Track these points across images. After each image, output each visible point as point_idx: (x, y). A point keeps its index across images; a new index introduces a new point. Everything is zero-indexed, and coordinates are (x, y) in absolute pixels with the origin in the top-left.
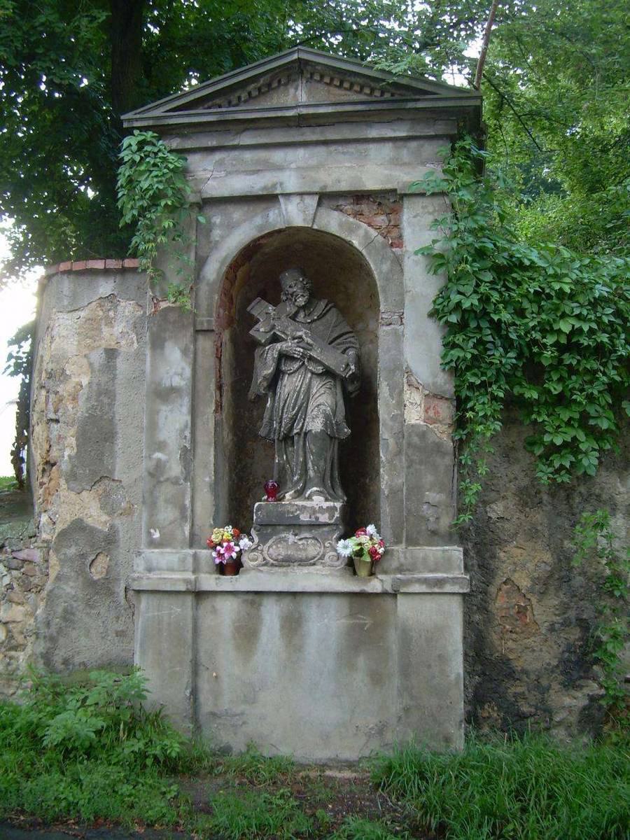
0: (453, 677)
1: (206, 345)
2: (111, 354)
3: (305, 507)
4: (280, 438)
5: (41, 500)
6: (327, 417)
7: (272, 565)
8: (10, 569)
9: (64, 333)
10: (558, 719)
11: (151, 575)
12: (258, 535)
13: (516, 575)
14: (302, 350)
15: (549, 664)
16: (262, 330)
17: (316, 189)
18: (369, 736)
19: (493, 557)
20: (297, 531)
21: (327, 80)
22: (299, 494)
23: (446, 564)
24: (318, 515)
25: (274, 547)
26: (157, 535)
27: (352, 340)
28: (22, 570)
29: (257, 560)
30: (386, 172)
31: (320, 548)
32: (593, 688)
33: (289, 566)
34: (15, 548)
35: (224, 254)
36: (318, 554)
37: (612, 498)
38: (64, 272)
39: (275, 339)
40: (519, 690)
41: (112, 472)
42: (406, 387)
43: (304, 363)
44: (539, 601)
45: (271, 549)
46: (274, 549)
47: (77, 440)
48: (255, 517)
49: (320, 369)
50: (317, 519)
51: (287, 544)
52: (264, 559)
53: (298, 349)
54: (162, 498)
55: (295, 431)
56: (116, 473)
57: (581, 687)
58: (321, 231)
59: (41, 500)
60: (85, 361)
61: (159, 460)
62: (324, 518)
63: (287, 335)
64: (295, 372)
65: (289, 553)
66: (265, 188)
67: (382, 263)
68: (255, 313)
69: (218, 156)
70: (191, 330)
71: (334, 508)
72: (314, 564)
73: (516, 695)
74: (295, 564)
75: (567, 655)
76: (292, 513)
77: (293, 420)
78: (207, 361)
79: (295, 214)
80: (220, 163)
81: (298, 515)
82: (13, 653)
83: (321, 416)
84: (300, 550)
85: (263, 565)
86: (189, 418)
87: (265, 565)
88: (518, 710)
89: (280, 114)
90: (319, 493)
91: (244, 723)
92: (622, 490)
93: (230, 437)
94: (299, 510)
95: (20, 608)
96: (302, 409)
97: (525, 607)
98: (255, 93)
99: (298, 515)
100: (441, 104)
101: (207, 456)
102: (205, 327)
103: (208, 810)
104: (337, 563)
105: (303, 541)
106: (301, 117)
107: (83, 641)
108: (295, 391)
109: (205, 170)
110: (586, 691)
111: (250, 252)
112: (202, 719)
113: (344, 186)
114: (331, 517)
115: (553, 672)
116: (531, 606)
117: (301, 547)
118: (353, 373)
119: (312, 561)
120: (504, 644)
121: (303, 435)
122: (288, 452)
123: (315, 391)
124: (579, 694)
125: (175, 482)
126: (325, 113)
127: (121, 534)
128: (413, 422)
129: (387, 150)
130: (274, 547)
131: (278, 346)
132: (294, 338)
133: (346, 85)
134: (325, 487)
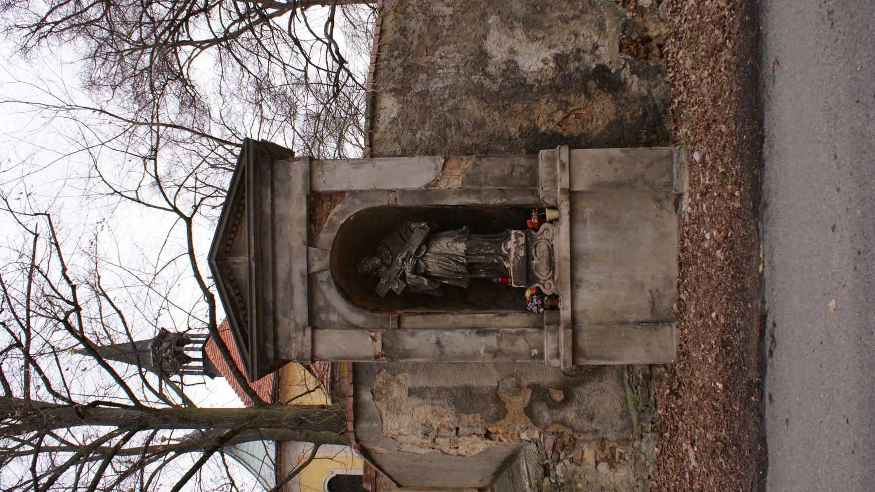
0: (622, 154)
1: (408, 321)
2: (411, 392)
3: (515, 253)
5: (511, 440)
6: (456, 241)
7: (553, 273)
8: (559, 461)
9: (397, 425)
10: (646, 93)
11: (562, 354)
13: (556, 120)
15: (612, 99)
16: (397, 286)
17: (305, 248)
18: (661, 208)
19: (544, 134)
21: (230, 242)
22: (506, 258)
23: (551, 160)
24: (520, 243)
26: (535, 351)
27: (404, 229)
28: (560, 451)
29: (550, 284)
30: (295, 201)
32: (626, 73)
34: (545, 457)
35: (347, 311)
37: (505, 63)
38: (355, 427)
39: (403, 277)
40: (628, 117)
41: (492, 388)
42: (437, 188)
43: (420, 258)
44: (572, 106)
46: (542, 273)
47: (470, 414)
49: (424, 247)
50: (522, 245)
52: (550, 278)
54: (510, 348)
56: (493, 385)
57: (625, 79)
58: (333, 245)
59: (511, 440)
60: (417, 409)
61: (485, 351)
62: (522, 241)
63: (401, 269)
64: (425, 264)
66: (303, 283)
67: (355, 205)
68: (386, 291)
69: (280, 316)
70: (398, 331)
71: (516, 234)
72: (552, 245)
73: (632, 118)
75: (605, 89)
76: (519, 261)
77: (457, 262)
78: (419, 320)
79: (321, 262)
80: (285, 314)
81: (521, 257)
82: (617, 456)
83: (455, 244)
84: (543, 255)
85: (554, 279)
86: (458, 331)
87: (553, 277)
88: (641, 117)
89: (254, 272)
90: (505, 245)
91: (657, 290)
92: (499, 57)
95: (585, 452)
96: (450, 257)
97: (576, 114)
98: (237, 291)
99: (521, 257)
100: (251, 165)
101: (482, 318)
104: (551, 230)
105: (537, 253)
106: (256, 259)
107: (607, 405)
108: (438, 263)
109: (289, 325)
110: (627, 76)
111: (347, 296)
112: (655, 319)
113: (304, 230)
114: (521, 236)
115: (616, 97)
116: (574, 110)
120: (598, 126)
123: (438, 250)
124: (630, 81)
125: (500, 340)
126: (232, 306)
127: (534, 380)
128: (460, 183)
129: (280, 202)
131: (408, 274)
132: (403, 264)
133: (234, 229)
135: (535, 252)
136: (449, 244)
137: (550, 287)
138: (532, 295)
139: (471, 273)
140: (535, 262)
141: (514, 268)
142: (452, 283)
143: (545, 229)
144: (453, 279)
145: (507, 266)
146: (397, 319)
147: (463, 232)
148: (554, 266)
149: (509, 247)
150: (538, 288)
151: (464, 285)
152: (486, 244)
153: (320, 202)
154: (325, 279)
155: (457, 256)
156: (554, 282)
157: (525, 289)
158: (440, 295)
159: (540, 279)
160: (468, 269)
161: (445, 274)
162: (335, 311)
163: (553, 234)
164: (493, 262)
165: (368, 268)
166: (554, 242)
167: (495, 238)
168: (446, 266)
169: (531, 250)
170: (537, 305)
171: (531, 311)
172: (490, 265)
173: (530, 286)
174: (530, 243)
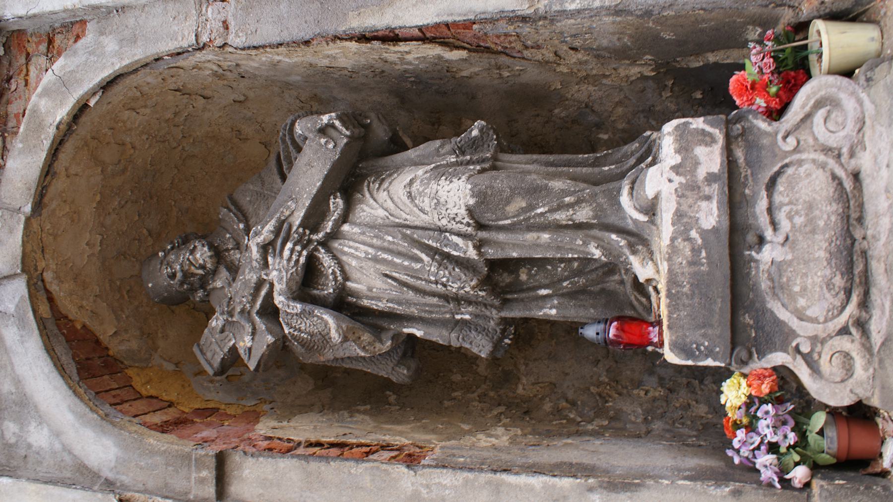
3: (679, 215)
4: (497, 302)
6: (440, 172)
7: (865, 304)
12: (762, 354)
14: (289, 245)
20: (751, 238)
24: (702, 173)
25: (802, 302)
29: (847, 356)
31: (800, 163)
33: (864, 253)
35: (70, 417)
36: (823, 166)
39: (270, 312)
45: (809, 313)
48: (710, 362)
49: (337, 204)
50: (711, 178)
51: (790, 263)
52: (844, 331)
53: (286, 253)
55: (472, 253)
65: (822, 254)
71: (682, 134)
72: (856, 176)
74: (858, 234)
76: (695, 251)
77: (444, 258)
81: (703, 233)
83: (434, 186)
84: (811, 221)
85: (865, 332)
87: (862, 325)
93: (500, 430)
94: (687, 231)
99: (703, 233)
102: (208, 474)
103: (263, 496)
104: (849, 104)
105: (781, 216)
108: (375, 260)
114: (706, 139)
117: (799, 220)
118: (339, 118)
119: (848, 185)
121: (483, 234)
122: (532, 283)
123: (381, 213)
130: (802, 302)
131: (279, 300)
132: (266, 265)
134: (622, 176)
135: (770, 210)
136: (416, 186)
137: (849, 371)
138: (750, 402)
139: (505, 303)
140: (767, 255)
141: (672, 281)
142: (438, 336)
143: (818, 105)
144: (443, 323)
145: (643, 272)
146: (212, 463)
147: (475, 145)
148: (866, 272)
149: (650, 192)
150: (783, 375)
151: (481, 347)
152: (557, 185)
153: (22, 60)
154: (11, 307)
155: (441, 230)
156: (867, 348)
157: (724, 374)
158: (401, 374)
159: (793, 334)
160: (487, 282)
161: (408, 303)
162: (42, 420)
163: (861, 123)
164: (587, 261)
165: (173, 276)
166: (864, 162)
167: (596, 163)
168: (407, 270)
169: (750, 202)
170: (773, 448)
171: (750, 469)
172: (579, 273)
173: (744, 363)
174: (744, 171)
